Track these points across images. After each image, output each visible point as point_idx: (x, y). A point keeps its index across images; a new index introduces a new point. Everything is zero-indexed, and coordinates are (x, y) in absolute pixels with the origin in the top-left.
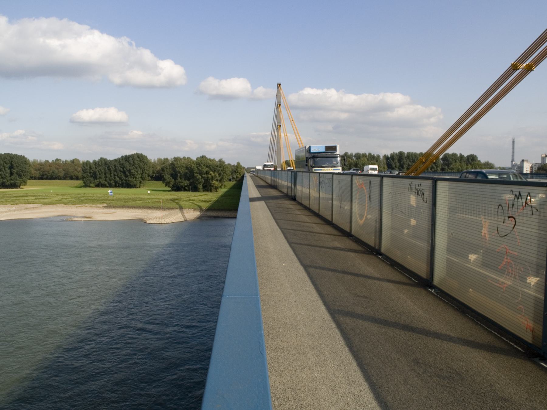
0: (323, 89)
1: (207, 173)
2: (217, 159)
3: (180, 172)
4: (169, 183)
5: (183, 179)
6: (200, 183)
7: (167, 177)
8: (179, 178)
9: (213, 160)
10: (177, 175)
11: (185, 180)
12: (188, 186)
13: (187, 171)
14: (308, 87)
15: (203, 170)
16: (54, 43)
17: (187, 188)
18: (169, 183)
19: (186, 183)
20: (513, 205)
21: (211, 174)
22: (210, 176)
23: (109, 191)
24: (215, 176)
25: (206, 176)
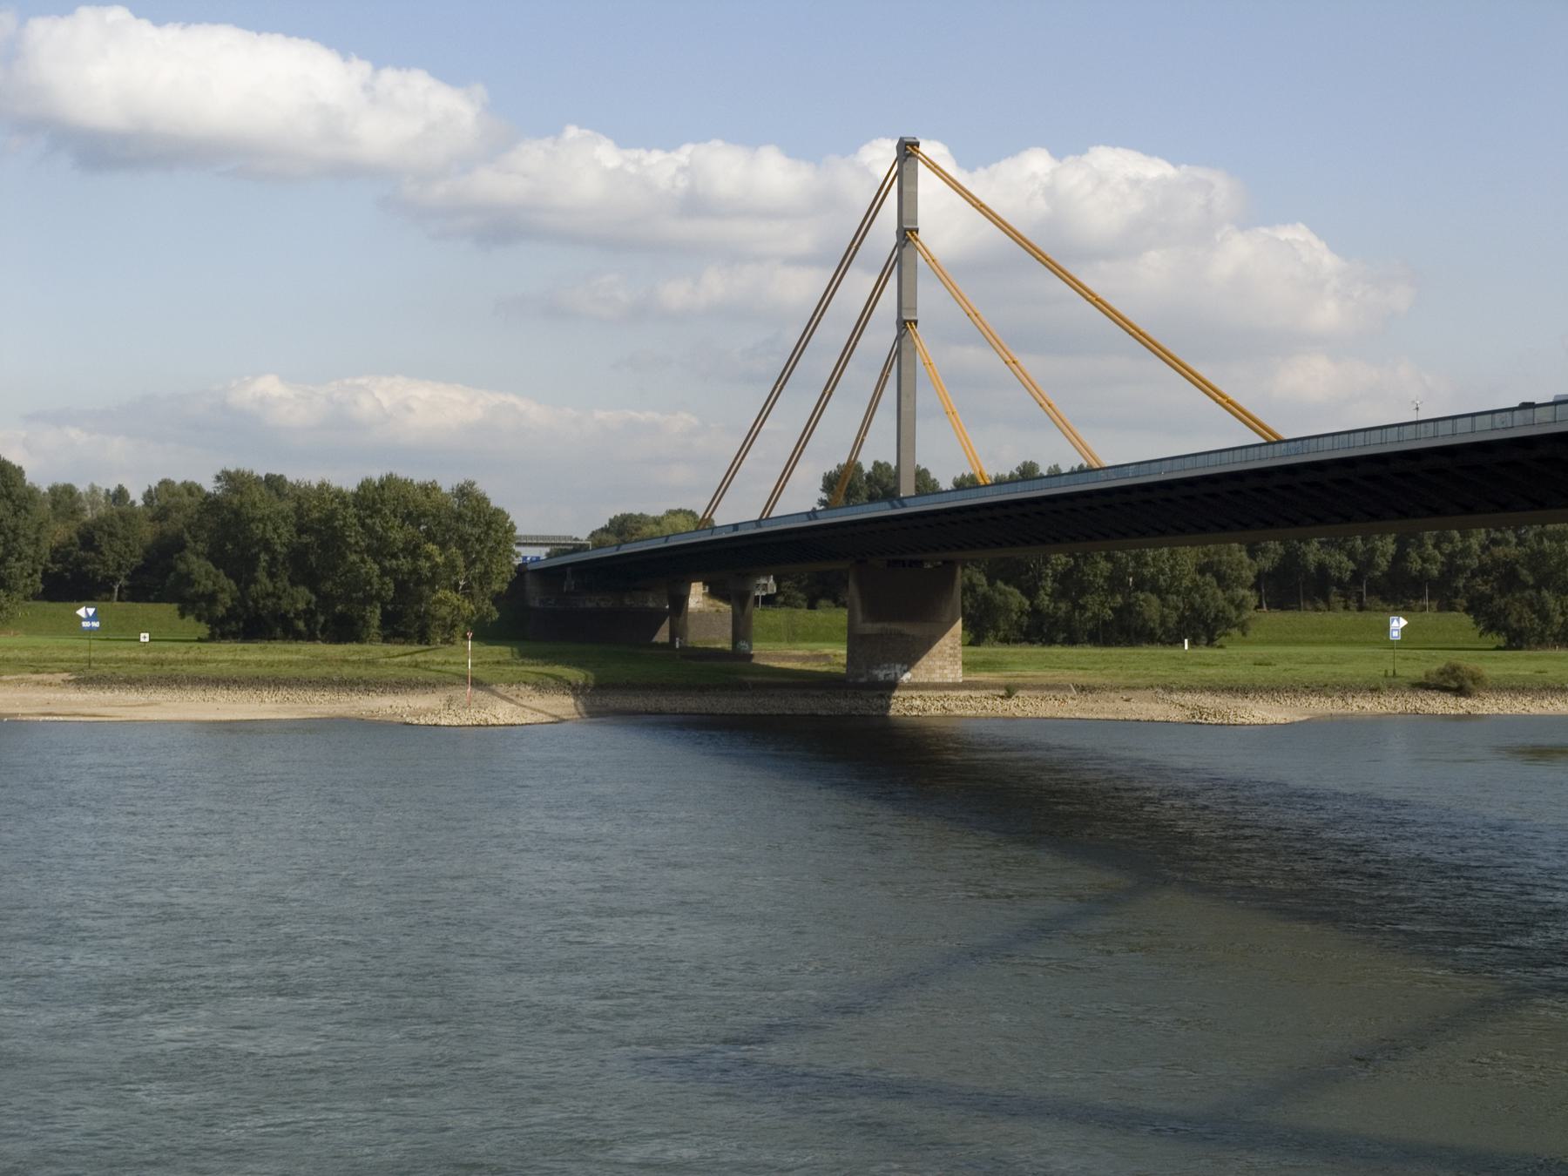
0: (670, 145)
1: (413, 550)
2: (447, 484)
3: (267, 546)
4: (211, 598)
5: (283, 582)
6: (368, 599)
7: (197, 565)
8: (261, 575)
9: (429, 490)
10: (256, 557)
11: (293, 583)
12: (309, 615)
13: (306, 539)
14: (1114, 141)
15: (393, 534)
16: (1479, 665)
17: (301, 625)
18: (211, 598)
19: (302, 597)
20: (134, 814)
21: (429, 557)
22: (424, 564)
23: (81, 612)
24: (451, 565)
25: (405, 563)
